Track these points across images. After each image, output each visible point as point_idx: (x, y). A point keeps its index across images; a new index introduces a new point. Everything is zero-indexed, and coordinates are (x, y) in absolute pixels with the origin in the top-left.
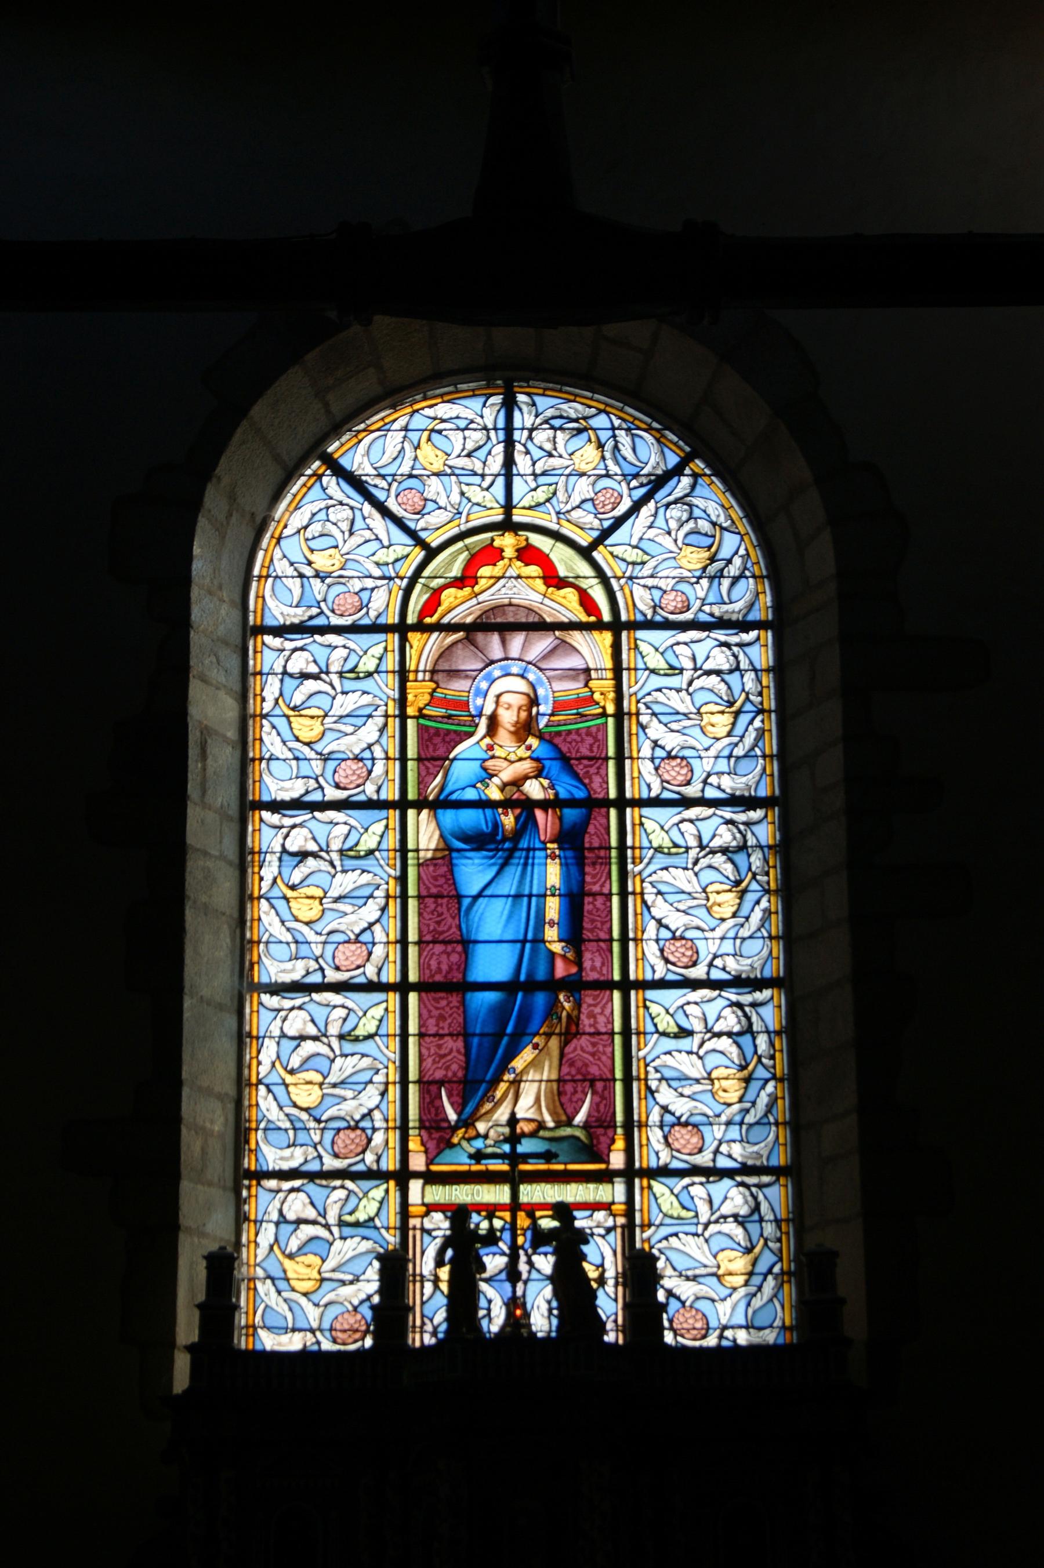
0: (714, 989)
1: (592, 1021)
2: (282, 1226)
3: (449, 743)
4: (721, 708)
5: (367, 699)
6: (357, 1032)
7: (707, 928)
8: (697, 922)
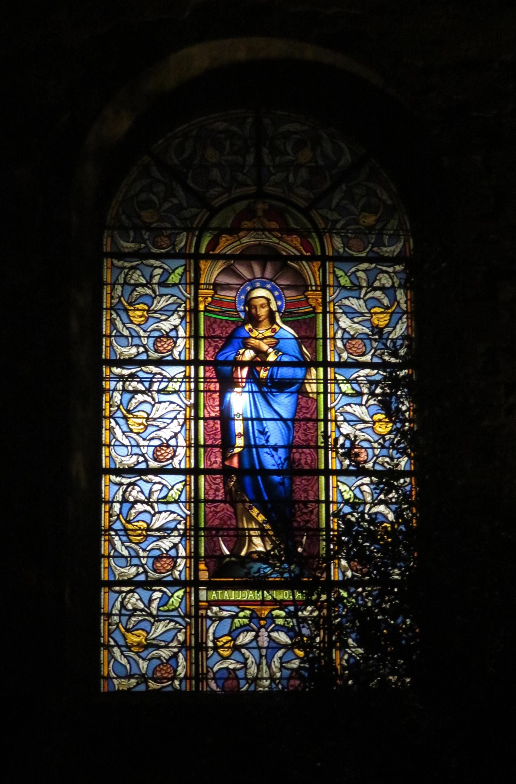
0: (373, 369)
1: (305, 495)
2: (125, 505)
3: (222, 327)
4: (382, 310)
5: (173, 516)
6: (168, 389)
7: (373, 441)
8: (367, 436)
